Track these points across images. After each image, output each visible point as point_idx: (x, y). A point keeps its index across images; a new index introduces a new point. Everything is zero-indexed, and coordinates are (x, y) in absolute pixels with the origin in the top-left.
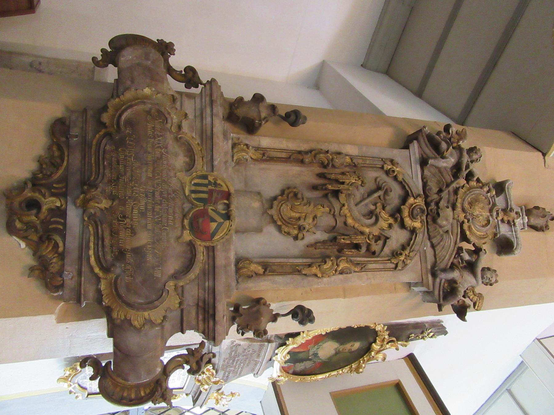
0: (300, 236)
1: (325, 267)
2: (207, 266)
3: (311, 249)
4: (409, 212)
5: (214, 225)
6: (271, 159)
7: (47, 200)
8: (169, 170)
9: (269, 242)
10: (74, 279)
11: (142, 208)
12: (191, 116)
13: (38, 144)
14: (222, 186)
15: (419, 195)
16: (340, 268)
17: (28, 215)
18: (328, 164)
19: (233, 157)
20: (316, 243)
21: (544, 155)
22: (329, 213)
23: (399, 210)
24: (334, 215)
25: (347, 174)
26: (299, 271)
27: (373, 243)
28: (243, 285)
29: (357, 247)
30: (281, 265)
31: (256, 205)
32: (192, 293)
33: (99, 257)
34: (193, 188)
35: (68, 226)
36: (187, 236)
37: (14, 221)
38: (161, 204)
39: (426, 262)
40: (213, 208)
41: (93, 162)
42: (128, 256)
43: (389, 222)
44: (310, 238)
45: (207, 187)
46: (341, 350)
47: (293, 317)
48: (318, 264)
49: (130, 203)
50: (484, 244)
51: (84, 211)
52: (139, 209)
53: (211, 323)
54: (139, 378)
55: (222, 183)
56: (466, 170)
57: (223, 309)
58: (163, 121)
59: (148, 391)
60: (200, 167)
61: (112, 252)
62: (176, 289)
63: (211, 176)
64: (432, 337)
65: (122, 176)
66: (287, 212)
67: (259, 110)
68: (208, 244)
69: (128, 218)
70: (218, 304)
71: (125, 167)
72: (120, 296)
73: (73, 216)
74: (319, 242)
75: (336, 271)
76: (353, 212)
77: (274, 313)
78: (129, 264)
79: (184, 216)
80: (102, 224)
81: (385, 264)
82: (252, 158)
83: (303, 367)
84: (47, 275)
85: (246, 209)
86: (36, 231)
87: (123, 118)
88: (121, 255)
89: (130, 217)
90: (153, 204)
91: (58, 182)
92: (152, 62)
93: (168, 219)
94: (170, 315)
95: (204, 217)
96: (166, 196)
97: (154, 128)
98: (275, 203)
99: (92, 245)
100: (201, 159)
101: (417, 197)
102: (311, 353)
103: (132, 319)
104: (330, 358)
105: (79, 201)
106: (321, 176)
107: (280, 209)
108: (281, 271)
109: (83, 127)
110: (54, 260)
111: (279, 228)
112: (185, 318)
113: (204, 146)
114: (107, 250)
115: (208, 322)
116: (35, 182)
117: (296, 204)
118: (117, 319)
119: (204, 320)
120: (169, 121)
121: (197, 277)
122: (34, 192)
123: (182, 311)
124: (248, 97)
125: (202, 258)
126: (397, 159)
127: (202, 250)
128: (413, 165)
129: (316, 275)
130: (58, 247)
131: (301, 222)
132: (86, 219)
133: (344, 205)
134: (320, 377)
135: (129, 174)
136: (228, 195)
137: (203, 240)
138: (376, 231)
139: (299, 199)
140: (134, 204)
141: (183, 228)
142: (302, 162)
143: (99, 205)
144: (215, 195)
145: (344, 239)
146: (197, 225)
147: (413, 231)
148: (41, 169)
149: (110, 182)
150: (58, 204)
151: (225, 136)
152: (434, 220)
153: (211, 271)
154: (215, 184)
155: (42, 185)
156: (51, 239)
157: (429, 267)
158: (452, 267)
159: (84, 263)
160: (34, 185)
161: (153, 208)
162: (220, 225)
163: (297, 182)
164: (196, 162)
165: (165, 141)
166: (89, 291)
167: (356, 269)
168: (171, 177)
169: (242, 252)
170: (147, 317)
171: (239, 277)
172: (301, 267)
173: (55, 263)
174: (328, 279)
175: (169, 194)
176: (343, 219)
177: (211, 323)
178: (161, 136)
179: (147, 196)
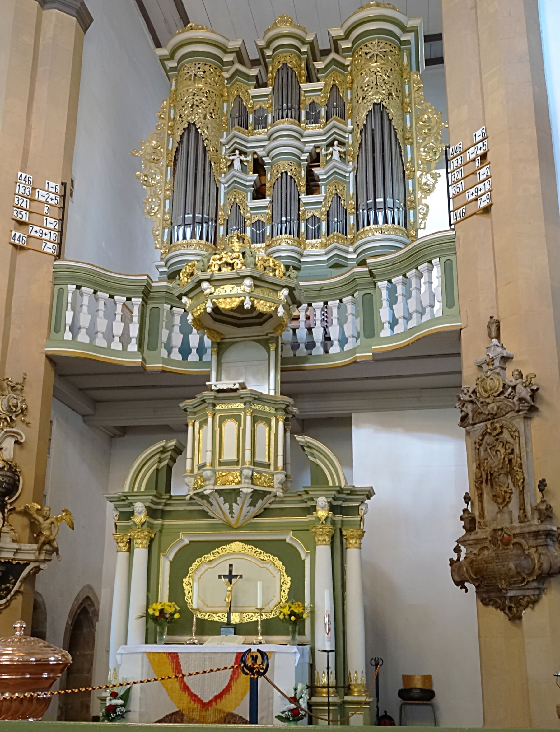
5: (505, 536)
12: (472, 549)
15: (486, 425)
21: (461, 329)
24: (499, 475)
29: (510, 461)
36: (511, 546)
39: (514, 416)
60: (487, 544)
68: (513, 537)
72: (532, 572)
73: (511, 594)
79: (504, 549)
88: (518, 573)
91: (501, 600)
111: (509, 502)
114: (518, 579)
116: (503, 610)
141: (507, 549)
159: (524, 587)
176: (500, 470)
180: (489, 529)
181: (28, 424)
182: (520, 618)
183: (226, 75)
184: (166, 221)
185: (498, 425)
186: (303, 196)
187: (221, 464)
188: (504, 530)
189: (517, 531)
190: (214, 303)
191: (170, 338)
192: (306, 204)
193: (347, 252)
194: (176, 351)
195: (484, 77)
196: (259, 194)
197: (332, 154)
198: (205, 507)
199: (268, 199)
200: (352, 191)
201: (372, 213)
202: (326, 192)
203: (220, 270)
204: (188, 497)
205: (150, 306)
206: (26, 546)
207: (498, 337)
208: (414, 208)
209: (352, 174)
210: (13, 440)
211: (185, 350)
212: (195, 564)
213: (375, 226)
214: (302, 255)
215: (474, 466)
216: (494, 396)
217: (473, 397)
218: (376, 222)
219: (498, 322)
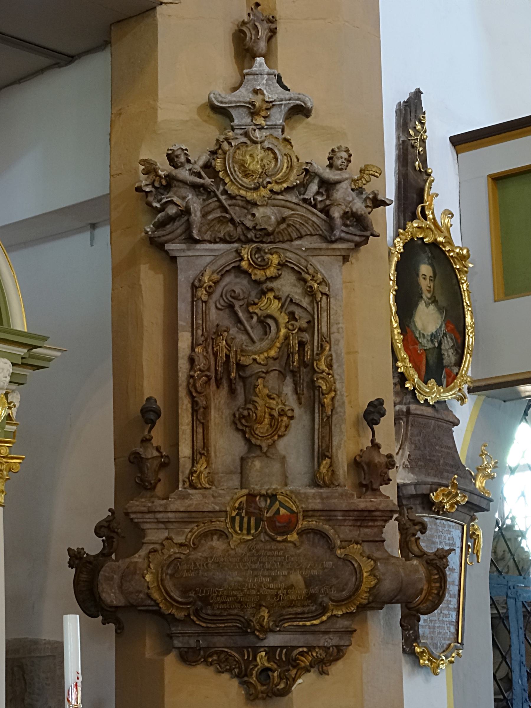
0: (290, 414)
1: (324, 388)
2: (322, 518)
3: (303, 401)
4: (260, 269)
5: (282, 511)
6: (206, 445)
7: (260, 664)
8: (229, 555)
9: (293, 446)
10: (332, 638)
11: (268, 580)
13: (203, 672)
14: (241, 502)
16: (326, 369)
17: (274, 678)
18: (207, 376)
19: (206, 488)
20: (297, 393)
22: (264, 378)
23: (258, 283)
24: (267, 373)
25: (215, 349)
26: (329, 417)
27: (297, 324)
28: (342, 480)
30: (322, 438)
31: (257, 464)
32: (347, 531)
33: (312, 617)
34: (245, 532)
35: (283, 645)
36: (293, 537)
37: (278, 689)
38: (264, 563)
40: (266, 511)
41: (223, 625)
42: (313, 591)
43: (272, 297)
44: (291, 401)
45: (243, 517)
46: (429, 295)
47: (377, 423)
48: (321, 396)
49: (263, 590)
50: (298, 160)
51: (272, 631)
52: (269, 583)
53: (377, 513)
54: (420, 580)
55: (239, 502)
56: (204, 179)
57: (363, 503)
58: (178, 561)
59: (436, 572)
61: (308, 606)
62: (344, 548)
63: (232, 513)
64: (423, 124)
65: (237, 599)
66: (263, 428)
67: (151, 458)
68: (300, 517)
69: (277, 592)
70: (359, 507)
71: (228, 596)
72: (349, 597)
73: (274, 640)
74: (296, 389)
75: (329, 374)
76: (261, 351)
77: (370, 445)
78: (320, 590)
80: (282, 615)
81: (323, 309)
82: (206, 468)
83: (451, 351)
84: (325, 661)
86: (288, 670)
87: (180, 600)
88: (311, 598)
89: (276, 591)
90: (264, 570)
92: (115, 574)
93: (278, 556)
94: (367, 553)
95: (275, 521)
96: (255, 558)
97: (188, 571)
98: (253, 441)
99: (301, 624)
100: (213, 523)
101: (240, 256)
102: (429, 346)
103: (369, 587)
104: (440, 309)
105: (261, 636)
106: (218, 384)
107: (255, 433)
108: (327, 439)
109: (189, 636)
110: (314, 654)
112: (371, 539)
113: (199, 520)
114: (306, 609)
115: (376, 516)
116: (242, 676)
117: (255, 418)
118: (368, 599)
119: (374, 520)
120: (178, 556)
121: (333, 527)
122: (252, 675)
123: (363, 541)
125: (314, 523)
126: (192, 274)
127: (306, 523)
128: (197, 254)
129: (333, 399)
130: (303, 651)
131: (276, 414)
132: (278, 629)
133: (255, 360)
134: (469, 320)
135: (236, 593)
136: (251, 496)
137: (298, 521)
138: (283, 319)
139: (249, 414)
140: (265, 587)
141: (285, 541)
142: (206, 408)
143: (266, 618)
144: (252, 510)
145: (293, 362)
146: (282, 527)
147: (282, 265)
148: (230, 671)
149: (242, 610)
150: (263, 654)
151: (184, 497)
152: (268, 234)
153: (328, 514)
154: (240, 508)
155: (246, 670)
156: (295, 658)
157: (324, 245)
158: (326, 211)
160: (246, 675)
161: (268, 570)
162: (282, 505)
163: (227, 412)
164: (218, 528)
165: (200, 560)
166: (344, 623)
167: (328, 348)
168: (236, 553)
169: (306, 480)
170: (368, 574)
171: (334, 484)
172: (324, 415)
173: (317, 653)
174: (337, 383)
175: (253, 555)
176: (271, 361)
177: (377, 513)
178: (195, 563)
179: (256, 576)
188: (279, 497)
216: (271, 191)
219: (272, 20)
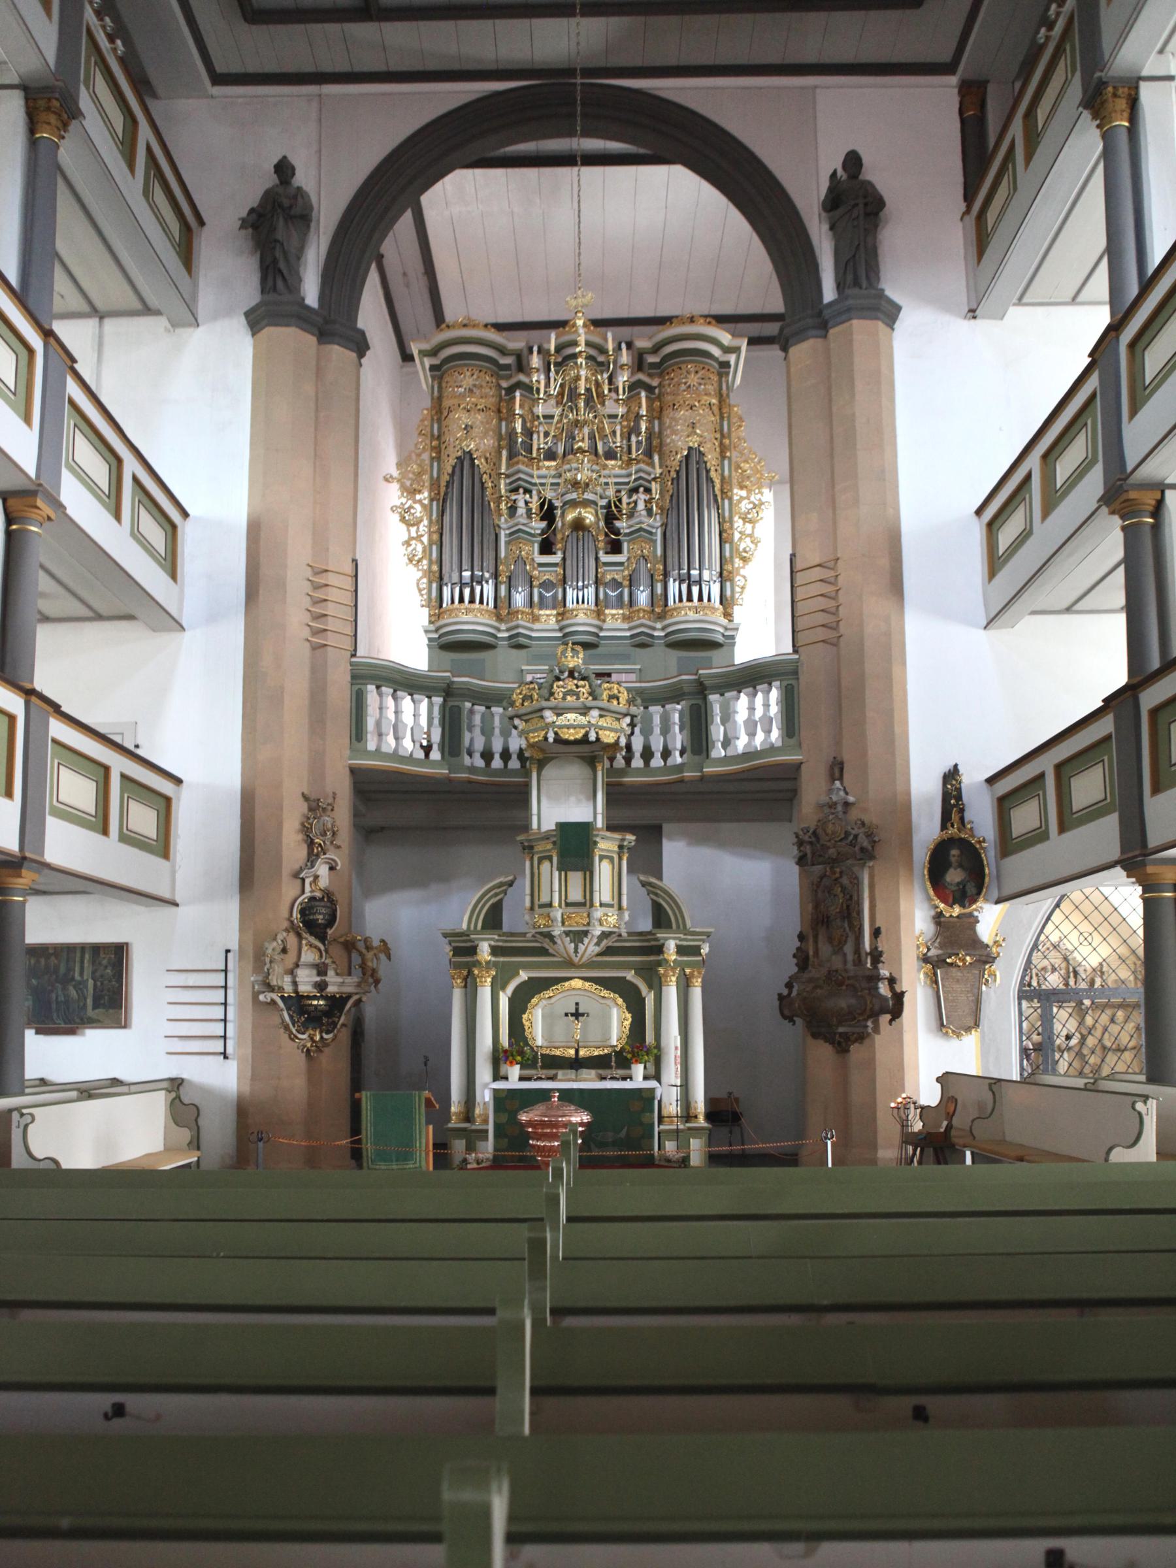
13: (821, 1042)
73: (841, 1030)
76: (834, 910)
85: (837, 963)
116: (832, 1043)
124: (795, 961)
147: (841, 873)
180: (824, 971)
181: (339, 847)
182: (848, 1051)
183: (504, 384)
184: (434, 572)
185: (838, 870)
186: (601, 553)
187: (567, 904)
189: (851, 974)
190: (556, 733)
191: (472, 740)
192: (606, 564)
193: (654, 629)
194: (477, 756)
195: (838, 488)
196: (547, 548)
197: (636, 502)
198: (547, 944)
199: (560, 555)
200: (659, 552)
201: (684, 587)
202: (629, 552)
203: (564, 698)
204: (529, 935)
205: (450, 704)
206: (349, 980)
207: (841, 779)
208: (732, 581)
209: (659, 531)
210: (327, 867)
211: (487, 756)
212: (534, 1000)
213: (690, 604)
214: (601, 629)
215: (810, 907)
217: (813, 839)
218: (690, 599)
219: (842, 763)
